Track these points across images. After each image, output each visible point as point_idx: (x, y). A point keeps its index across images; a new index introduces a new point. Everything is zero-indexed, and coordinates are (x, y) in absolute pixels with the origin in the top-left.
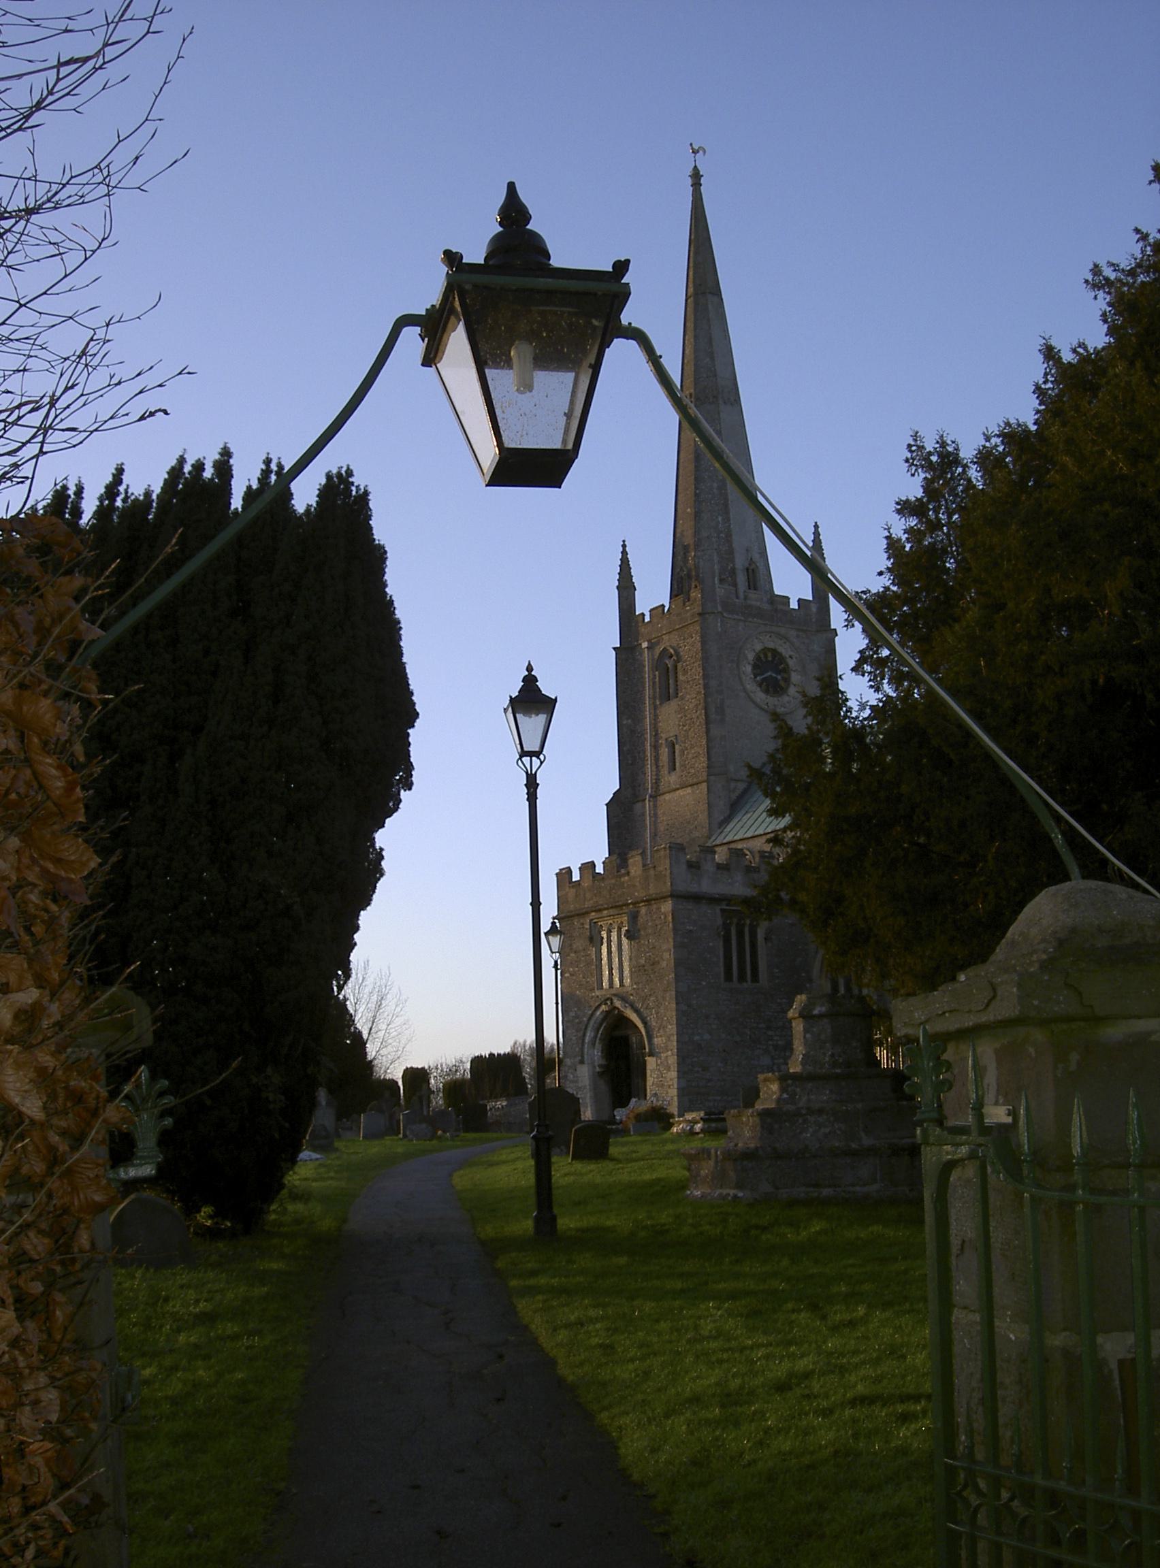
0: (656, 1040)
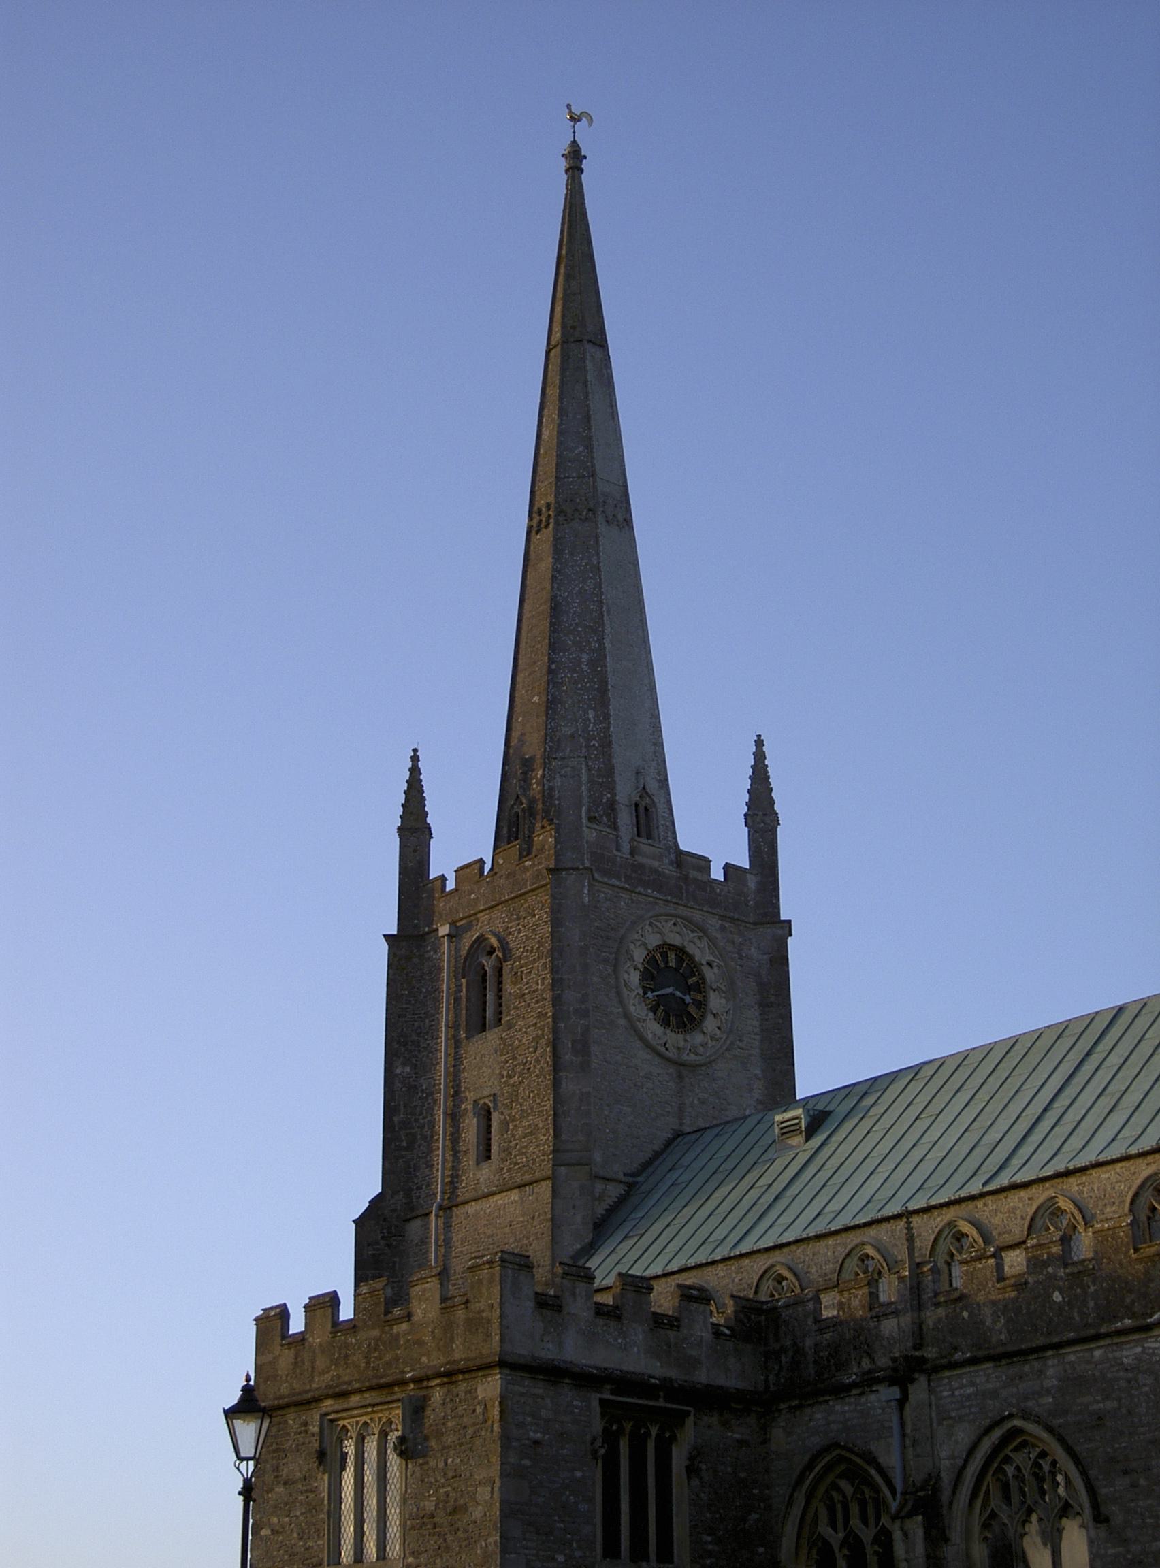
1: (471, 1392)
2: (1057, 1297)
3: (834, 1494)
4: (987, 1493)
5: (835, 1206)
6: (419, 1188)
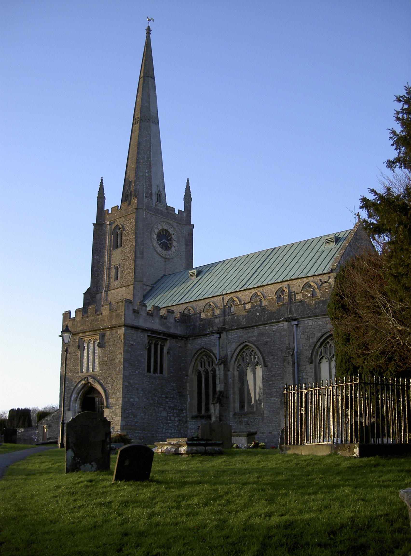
0: (110, 400)
1: (117, 332)
2: (258, 314)
3: (202, 359)
4: (239, 359)
5: (203, 293)
6: (100, 286)
